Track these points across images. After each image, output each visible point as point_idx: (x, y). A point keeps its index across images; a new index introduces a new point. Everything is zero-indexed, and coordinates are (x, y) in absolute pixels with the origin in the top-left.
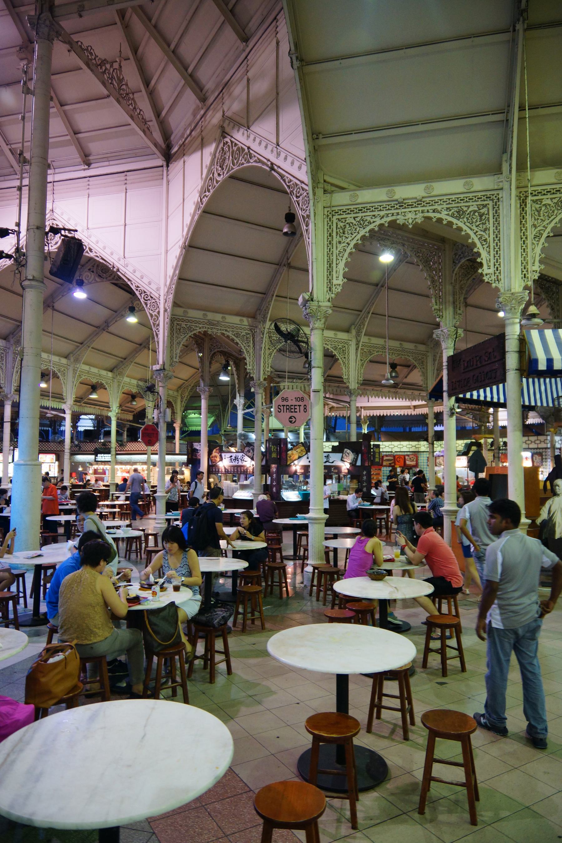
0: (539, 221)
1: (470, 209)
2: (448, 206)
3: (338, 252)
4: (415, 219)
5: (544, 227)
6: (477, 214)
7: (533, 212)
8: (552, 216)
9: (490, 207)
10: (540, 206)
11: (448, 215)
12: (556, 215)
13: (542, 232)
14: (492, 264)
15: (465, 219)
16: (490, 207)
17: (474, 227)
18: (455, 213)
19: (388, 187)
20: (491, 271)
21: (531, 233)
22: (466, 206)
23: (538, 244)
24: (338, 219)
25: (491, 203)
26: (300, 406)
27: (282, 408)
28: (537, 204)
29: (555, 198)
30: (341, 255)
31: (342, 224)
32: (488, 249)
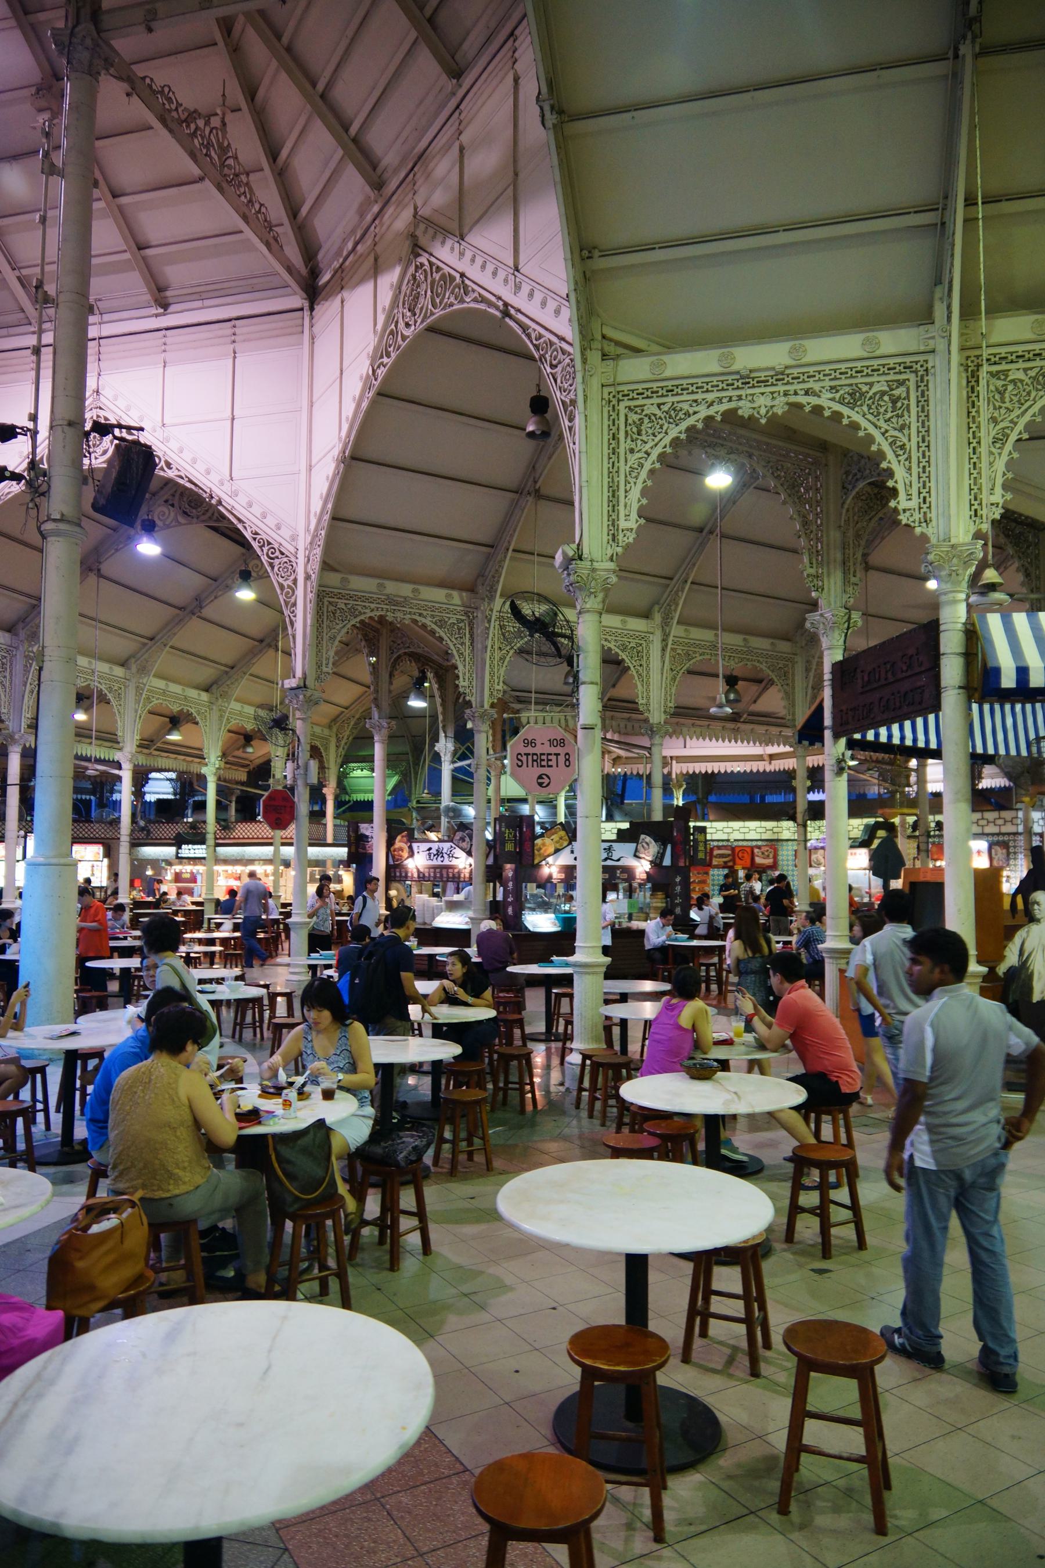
0: (1003, 411)
1: (875, 389)
2: (833, 383)
3: (628, 469)
4: (772, 407)
5: (1011, 421)
6: (886, 398)
7: (991, 395)
8: (1026, 401)
9: (912, 385)
10: (1003, 383)
11: (833, 399)
12: (1034, 399)
13: (1007, 431)
14: (914, 491)
15: (865, 408)
16: (912, 385)
17: (881, 423)
18: (846, 396)
19: (721, 348)
20: (914, 504)
21: (987, 433)
22: (866, 384)
23: (1000, 454)
24: (629, 408)
25: (912, 377)
26: (557, 755)
27: (524, 758)
28: (999, 379)
29: (1031, 369)
30: (634, 475)
31: (636, 417)
32: (907, 463)
